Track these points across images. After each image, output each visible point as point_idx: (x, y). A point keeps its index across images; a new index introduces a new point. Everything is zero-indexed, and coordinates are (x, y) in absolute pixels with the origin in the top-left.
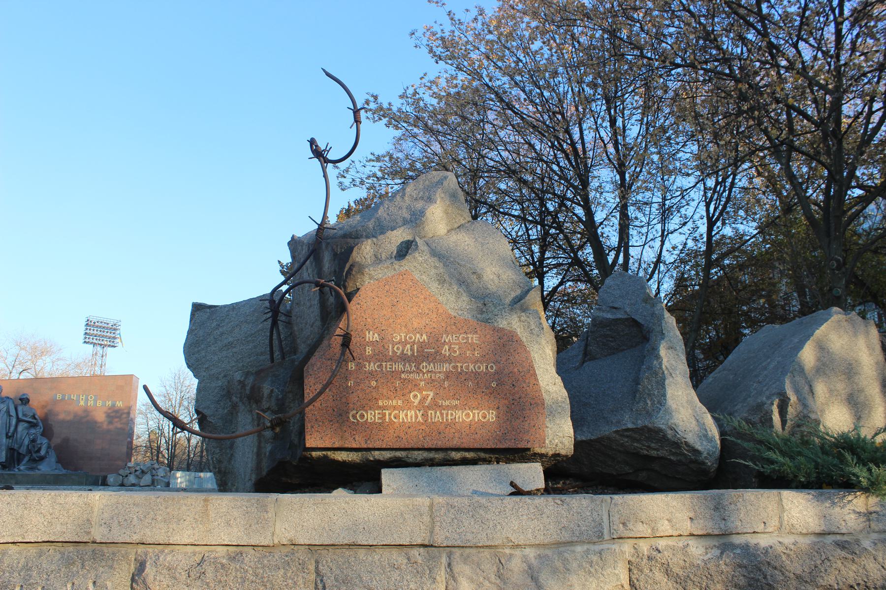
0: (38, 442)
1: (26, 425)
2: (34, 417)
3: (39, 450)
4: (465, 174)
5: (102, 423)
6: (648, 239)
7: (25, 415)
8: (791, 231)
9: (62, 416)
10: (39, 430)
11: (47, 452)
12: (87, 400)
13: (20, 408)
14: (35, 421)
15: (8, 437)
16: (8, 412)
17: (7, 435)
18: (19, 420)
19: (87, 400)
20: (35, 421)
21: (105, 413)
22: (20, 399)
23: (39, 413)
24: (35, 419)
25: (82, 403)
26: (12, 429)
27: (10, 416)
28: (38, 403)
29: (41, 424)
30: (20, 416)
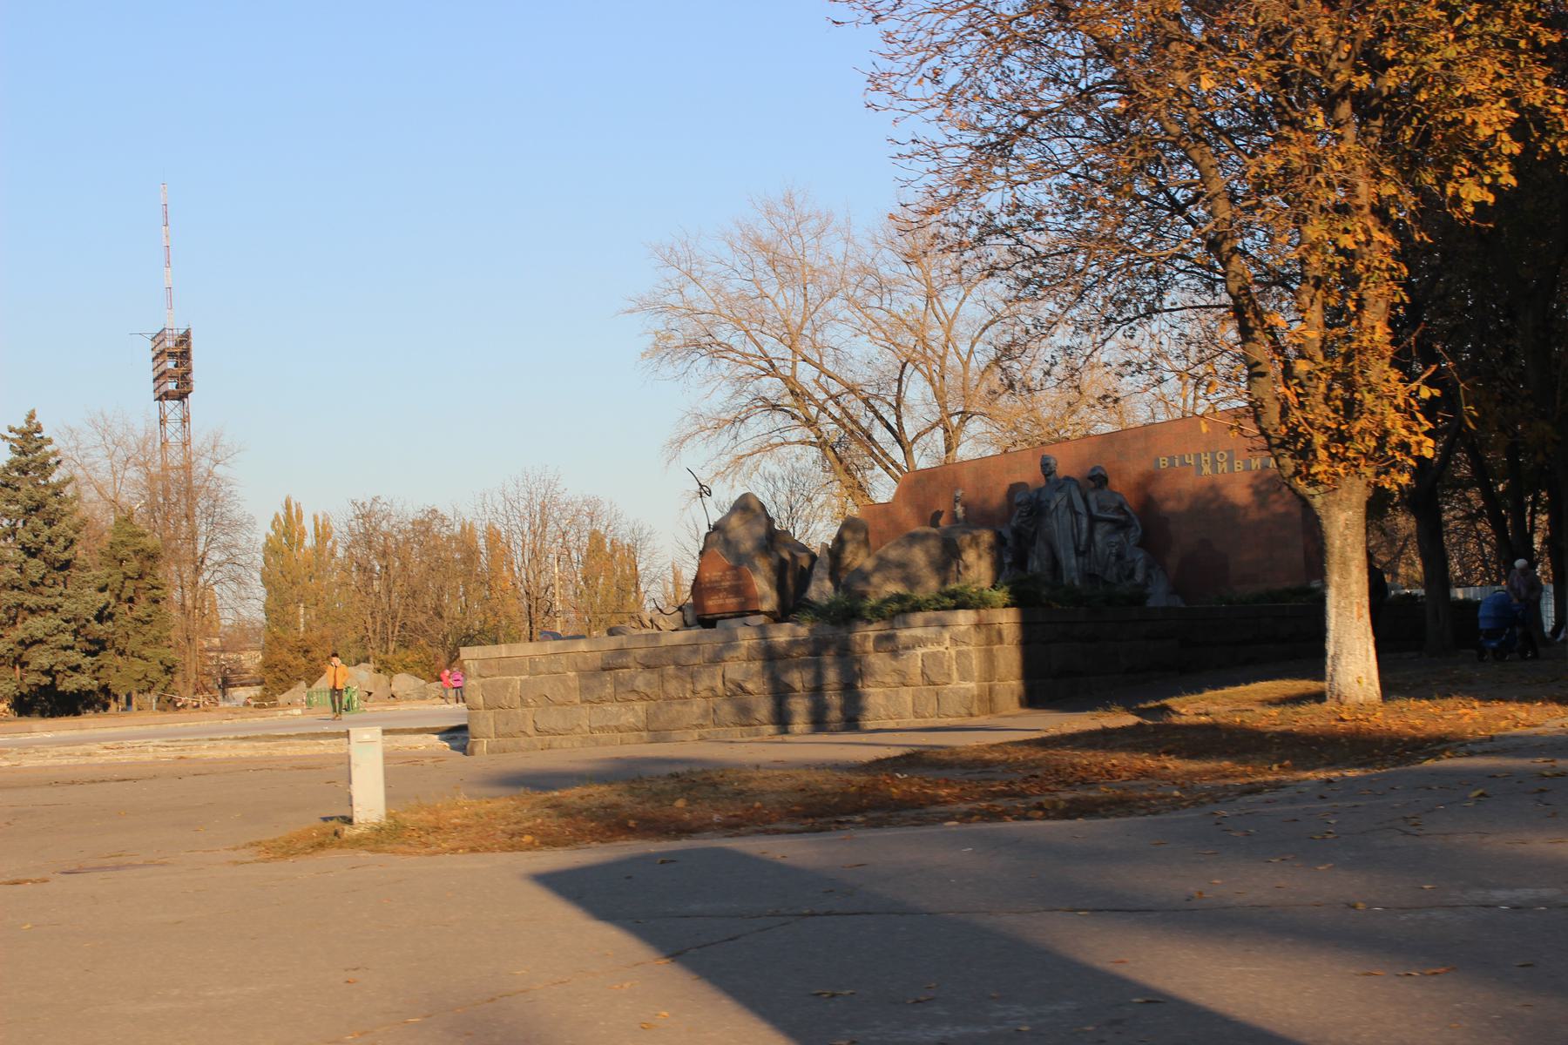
0: (1128, 558)
1: (1108, 527)
2: (1120, 508)
3: (1131, 575)
4: (210, 474)
5: (1246, 508)
6: (965, 357)
7: (1101, 508)
8: (1436, 342)
9: (1170, 505)
10: (1135, 533)
11: (1148, 576)
12: (1214, 462)
13: (1092, 496)
14: (1122, 517)
15: (1078, 553)
16: (1070, 505)
17: (1076, 549)
18: (1093, 520)
19: (1214, 462)
20: (1122, 517)
21: (1250, 486)
22: (1091, 478)
23: (1131, 501)
24: (1125, 512)
25: (1207, 469)
26: (1084, 537)
27: (1077, 513)
28: (1127, 473)
29: (1137, 523)
30: (1094, 510)
